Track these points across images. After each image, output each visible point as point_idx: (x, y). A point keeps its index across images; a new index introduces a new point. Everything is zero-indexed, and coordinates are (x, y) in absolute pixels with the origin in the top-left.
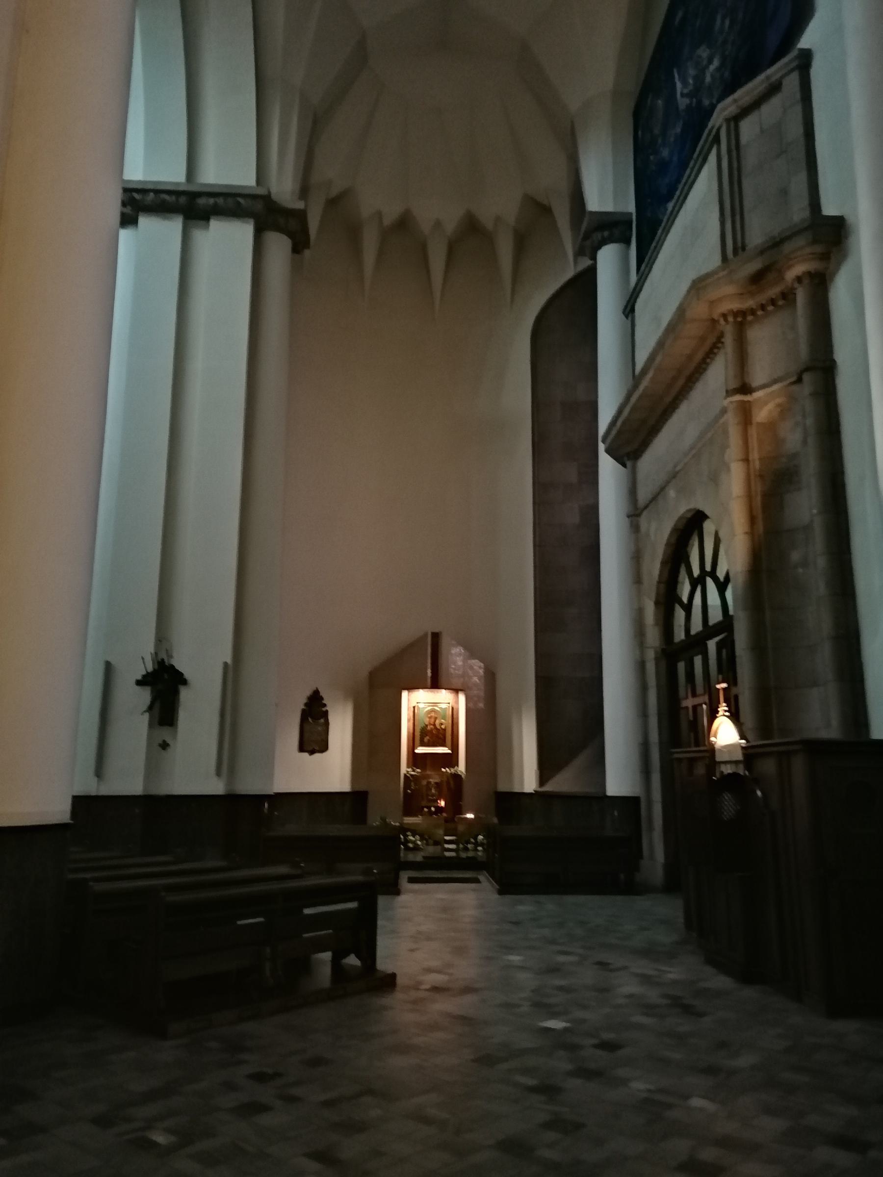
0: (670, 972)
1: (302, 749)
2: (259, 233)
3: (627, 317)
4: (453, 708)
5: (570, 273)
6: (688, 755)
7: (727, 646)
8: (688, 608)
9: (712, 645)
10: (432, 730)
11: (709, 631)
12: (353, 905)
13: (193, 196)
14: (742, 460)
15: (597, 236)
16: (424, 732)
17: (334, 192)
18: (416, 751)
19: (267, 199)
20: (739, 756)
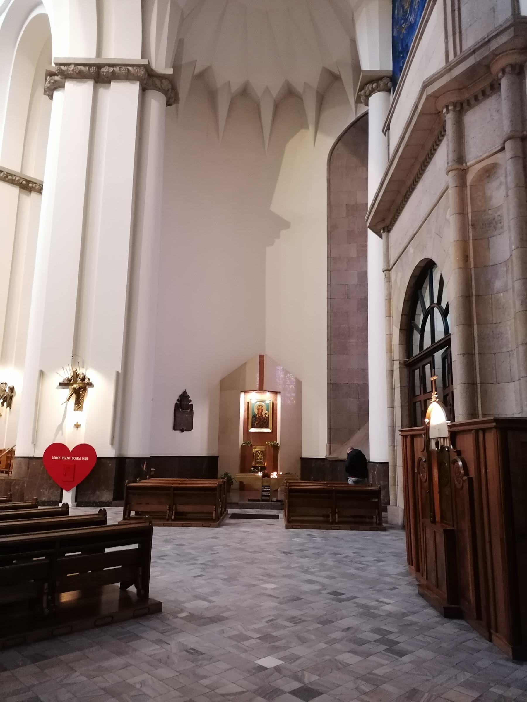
0: (388, 604)
1: (175, 429)
2: (143, 90)
3: (385, 134)
4: (273, 404)
5: (352, 118)
6: (411, 433)
7: (447, 358)
8: (422, 332)
9: (438, 356)
10: (259, 417)
11: (436, 347)
12: (135, 546)
13: (99, 67)
14: (459, 214)
15: (369, 87)
16: (254, 417)
17: (198, 70)
18: (249, 431)
19: (148, 68)
20: (446, 434)
